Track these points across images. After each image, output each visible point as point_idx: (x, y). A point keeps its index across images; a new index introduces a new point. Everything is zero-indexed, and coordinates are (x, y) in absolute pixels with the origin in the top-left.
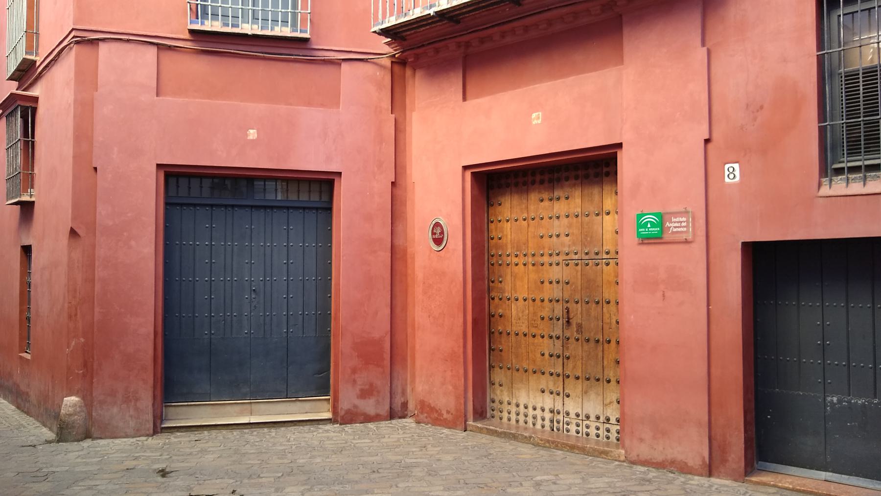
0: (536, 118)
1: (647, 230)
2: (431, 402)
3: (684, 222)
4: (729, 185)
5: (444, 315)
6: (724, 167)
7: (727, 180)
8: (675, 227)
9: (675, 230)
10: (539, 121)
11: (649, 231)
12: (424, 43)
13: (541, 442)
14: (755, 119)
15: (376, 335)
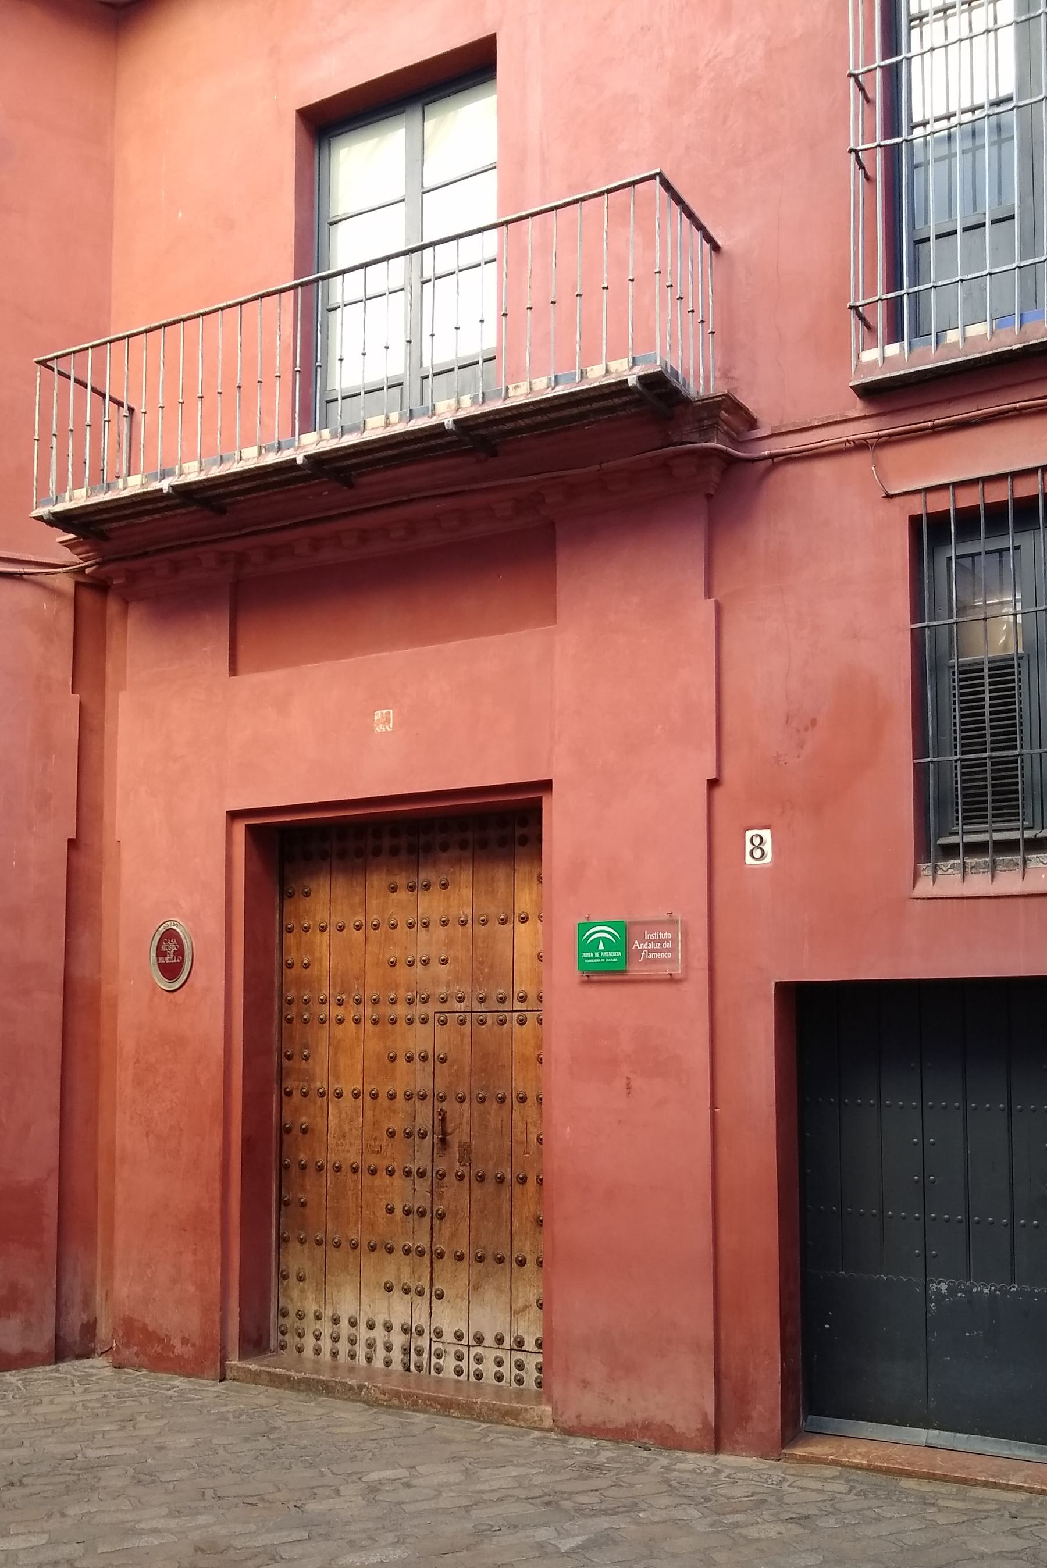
2: (147, 1320)
4: (753, 870)
7: (749, 860)
8: (651, 951)
9: (650, 956)
10: (389, 728)
11: (600, 958)
13: (382, 1397)
14: (801, 745)
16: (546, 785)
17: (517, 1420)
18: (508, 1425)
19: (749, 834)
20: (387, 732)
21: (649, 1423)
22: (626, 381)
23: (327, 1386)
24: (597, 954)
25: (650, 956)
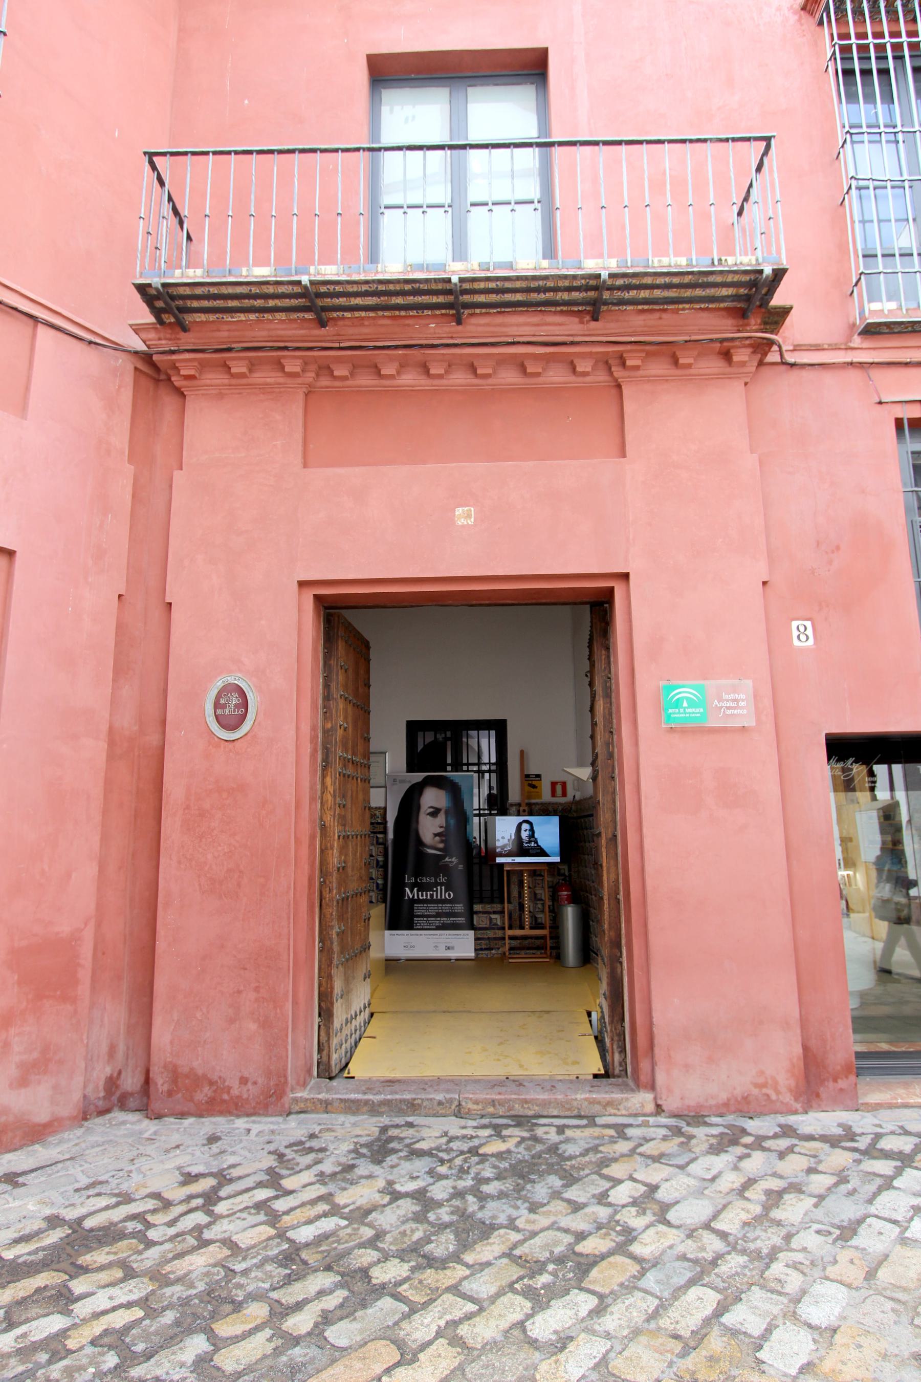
0: (464, 516)
1: (682, 710)
2: (195, 1064)
3: (743, 700)
4: (802, 650)
5: (241, 872)
6: (790, 626)
7: (796, 643)
8: (728, 708)
9: (729, 712)
10: (471, 521)
11: (686, 713)
12: (233, 346)
13: (475, 1107)
14: (830, 562)
15: (64, 927)
16: (625, 577)
17: (619, 1110)
18: (610, 1115)
19: (795, 624)
20: (468, 525)
21: (748, 1095)
22: (600, 275)
23: (413, 1105)
24: (682, 710)
25: (729, 712)
